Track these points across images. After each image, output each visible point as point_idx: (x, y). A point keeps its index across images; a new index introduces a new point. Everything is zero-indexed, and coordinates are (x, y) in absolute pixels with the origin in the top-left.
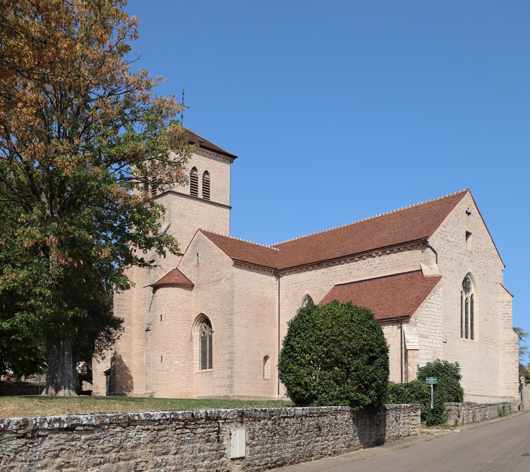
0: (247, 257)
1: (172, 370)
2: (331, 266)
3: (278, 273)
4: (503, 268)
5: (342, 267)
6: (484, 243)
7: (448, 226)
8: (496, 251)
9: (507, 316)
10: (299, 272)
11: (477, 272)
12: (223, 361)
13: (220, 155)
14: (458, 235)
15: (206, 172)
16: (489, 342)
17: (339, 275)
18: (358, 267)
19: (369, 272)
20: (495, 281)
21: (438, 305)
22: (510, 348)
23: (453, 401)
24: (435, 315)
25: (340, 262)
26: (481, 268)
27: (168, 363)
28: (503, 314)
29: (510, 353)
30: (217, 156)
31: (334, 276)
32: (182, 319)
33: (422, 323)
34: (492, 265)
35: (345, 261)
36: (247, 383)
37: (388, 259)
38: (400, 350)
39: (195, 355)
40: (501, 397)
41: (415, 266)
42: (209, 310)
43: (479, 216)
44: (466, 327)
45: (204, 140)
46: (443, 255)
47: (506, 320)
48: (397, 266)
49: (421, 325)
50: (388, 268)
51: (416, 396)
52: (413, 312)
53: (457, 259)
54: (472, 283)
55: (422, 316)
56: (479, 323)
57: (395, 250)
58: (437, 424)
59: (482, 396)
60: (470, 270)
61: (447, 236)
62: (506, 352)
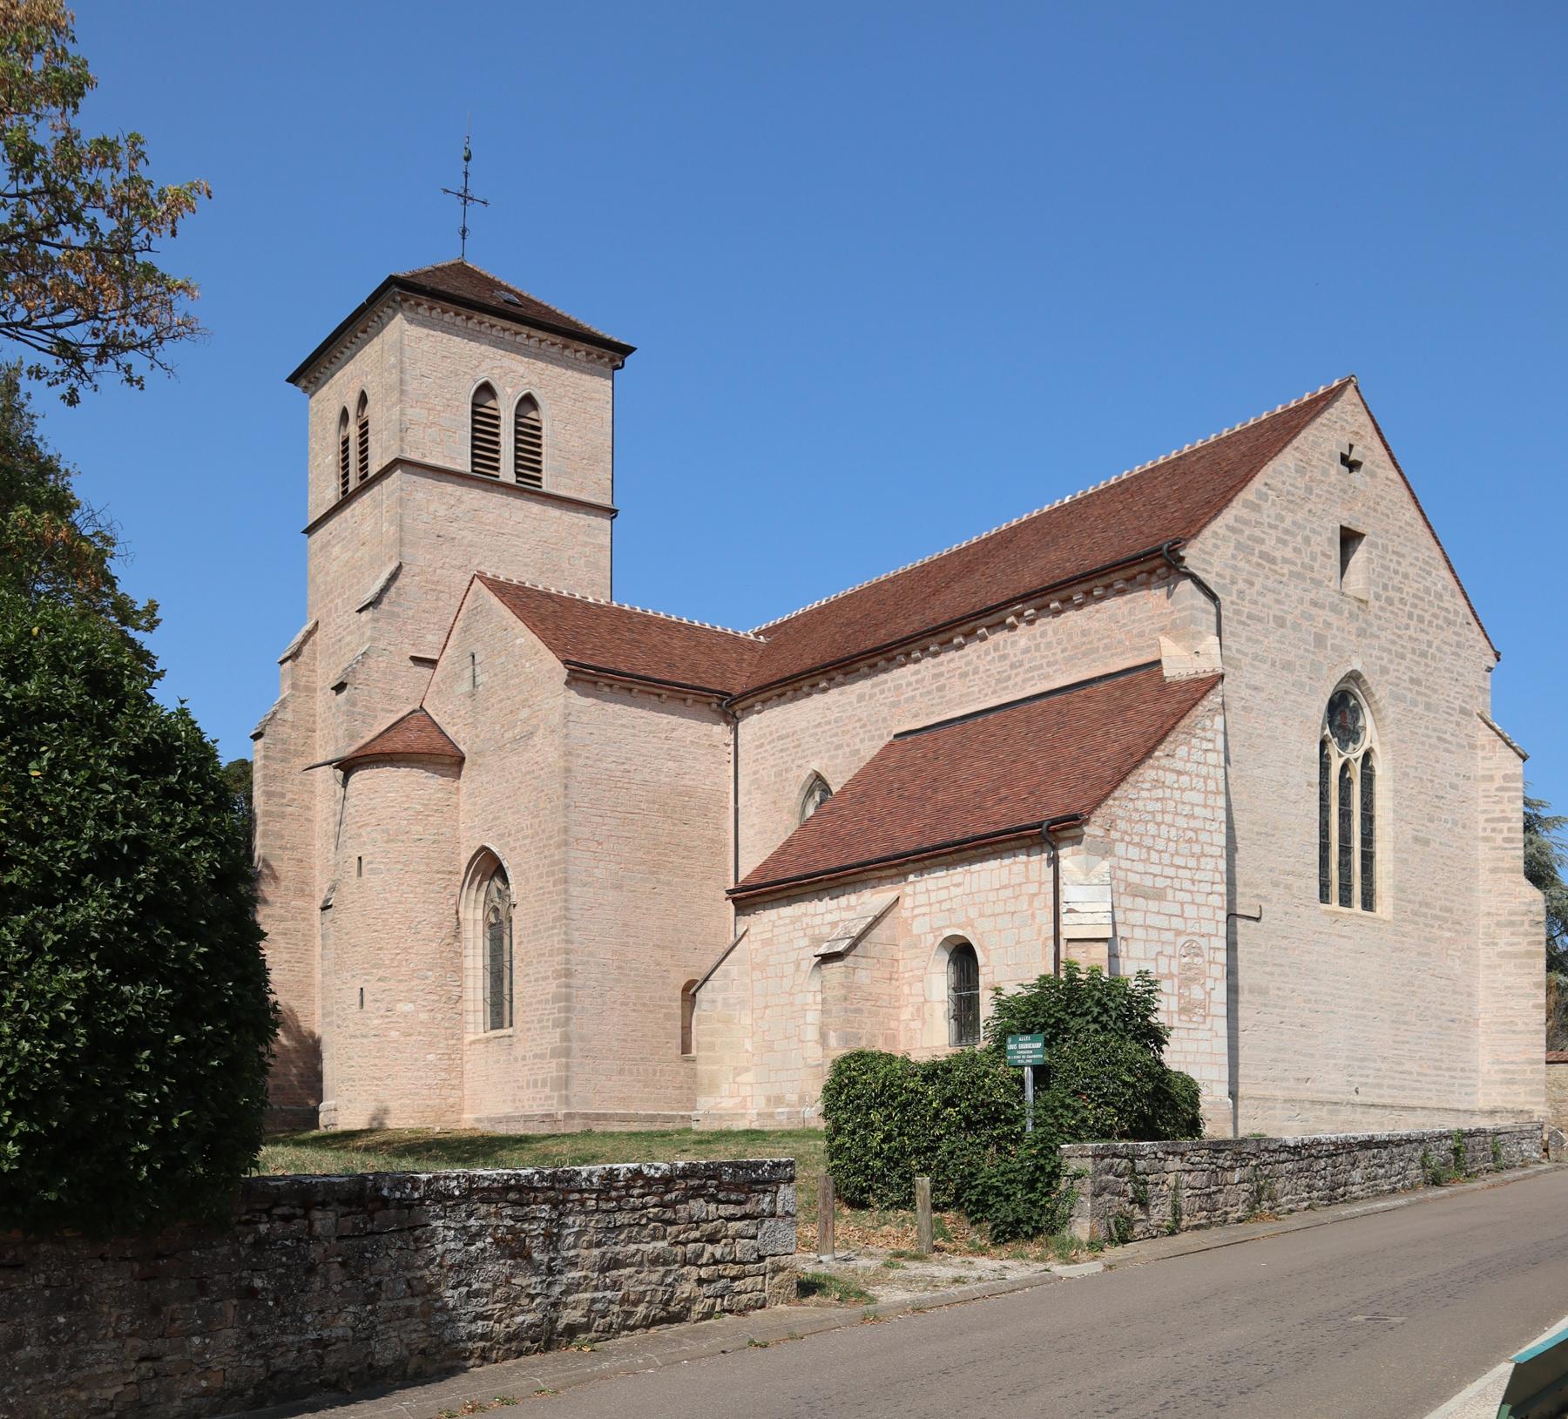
0: (612, 657)
1: (394, 1034)
2: (885, 670)
3: (728, 707)
4: (1492, 662)
5: (917, 672)
6: (1412, 571)
7: (1265, 506)
8: (1463, 602)
9: (1505, 826)
10: (791, 701)
11: (1384, 671)
12: (540, 1002)
13: (576, 344)
14: (1307, 540)
15: (528, 401)
16: (1435, 917)
17: (907, 700)
18: (965, 669)
19: (999, 681)
20: (1457, 704)
21: (1206, 778)
22: (1515, 939)
23: (1123, 1135)
24: (1192, 816)
25: (908, 655)
26: (1403, 657)
27: (382, 1012)
28: (1487, 820)
29: (1515, 956)
30: (565, 347)
31: (895, 705)
32: (422, 868)
33: (1138, 845)
34: (1446, 648)
35: (924, 650)
36: (621, 1072)
37: (1055, 632)
38: (1051, 943)
39: (470, 983)
40: (1482, 1112)
41: (1140, 649)
42: (501, 836)
43: (1394, 475)
44: (1345, 865)
45: (519, 296)
46: (1246, 608)
47: (1499, 842)
48: (1085, 655)
49: (1133, 852)
50: (1056, 662)
51: (967, 1118)
52: (1098, 803)
53: (1306, 624)
54: (1367, 710)
55: (1136, 816)
56: (1395, 850)
57: (1077, 598)
58: (1029, 1237)
59: (1405, 1108)
60: (1357, 665)
61: (1262, 541)
62: (1502, 955)
